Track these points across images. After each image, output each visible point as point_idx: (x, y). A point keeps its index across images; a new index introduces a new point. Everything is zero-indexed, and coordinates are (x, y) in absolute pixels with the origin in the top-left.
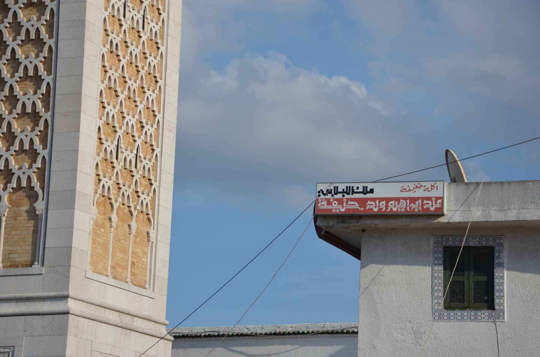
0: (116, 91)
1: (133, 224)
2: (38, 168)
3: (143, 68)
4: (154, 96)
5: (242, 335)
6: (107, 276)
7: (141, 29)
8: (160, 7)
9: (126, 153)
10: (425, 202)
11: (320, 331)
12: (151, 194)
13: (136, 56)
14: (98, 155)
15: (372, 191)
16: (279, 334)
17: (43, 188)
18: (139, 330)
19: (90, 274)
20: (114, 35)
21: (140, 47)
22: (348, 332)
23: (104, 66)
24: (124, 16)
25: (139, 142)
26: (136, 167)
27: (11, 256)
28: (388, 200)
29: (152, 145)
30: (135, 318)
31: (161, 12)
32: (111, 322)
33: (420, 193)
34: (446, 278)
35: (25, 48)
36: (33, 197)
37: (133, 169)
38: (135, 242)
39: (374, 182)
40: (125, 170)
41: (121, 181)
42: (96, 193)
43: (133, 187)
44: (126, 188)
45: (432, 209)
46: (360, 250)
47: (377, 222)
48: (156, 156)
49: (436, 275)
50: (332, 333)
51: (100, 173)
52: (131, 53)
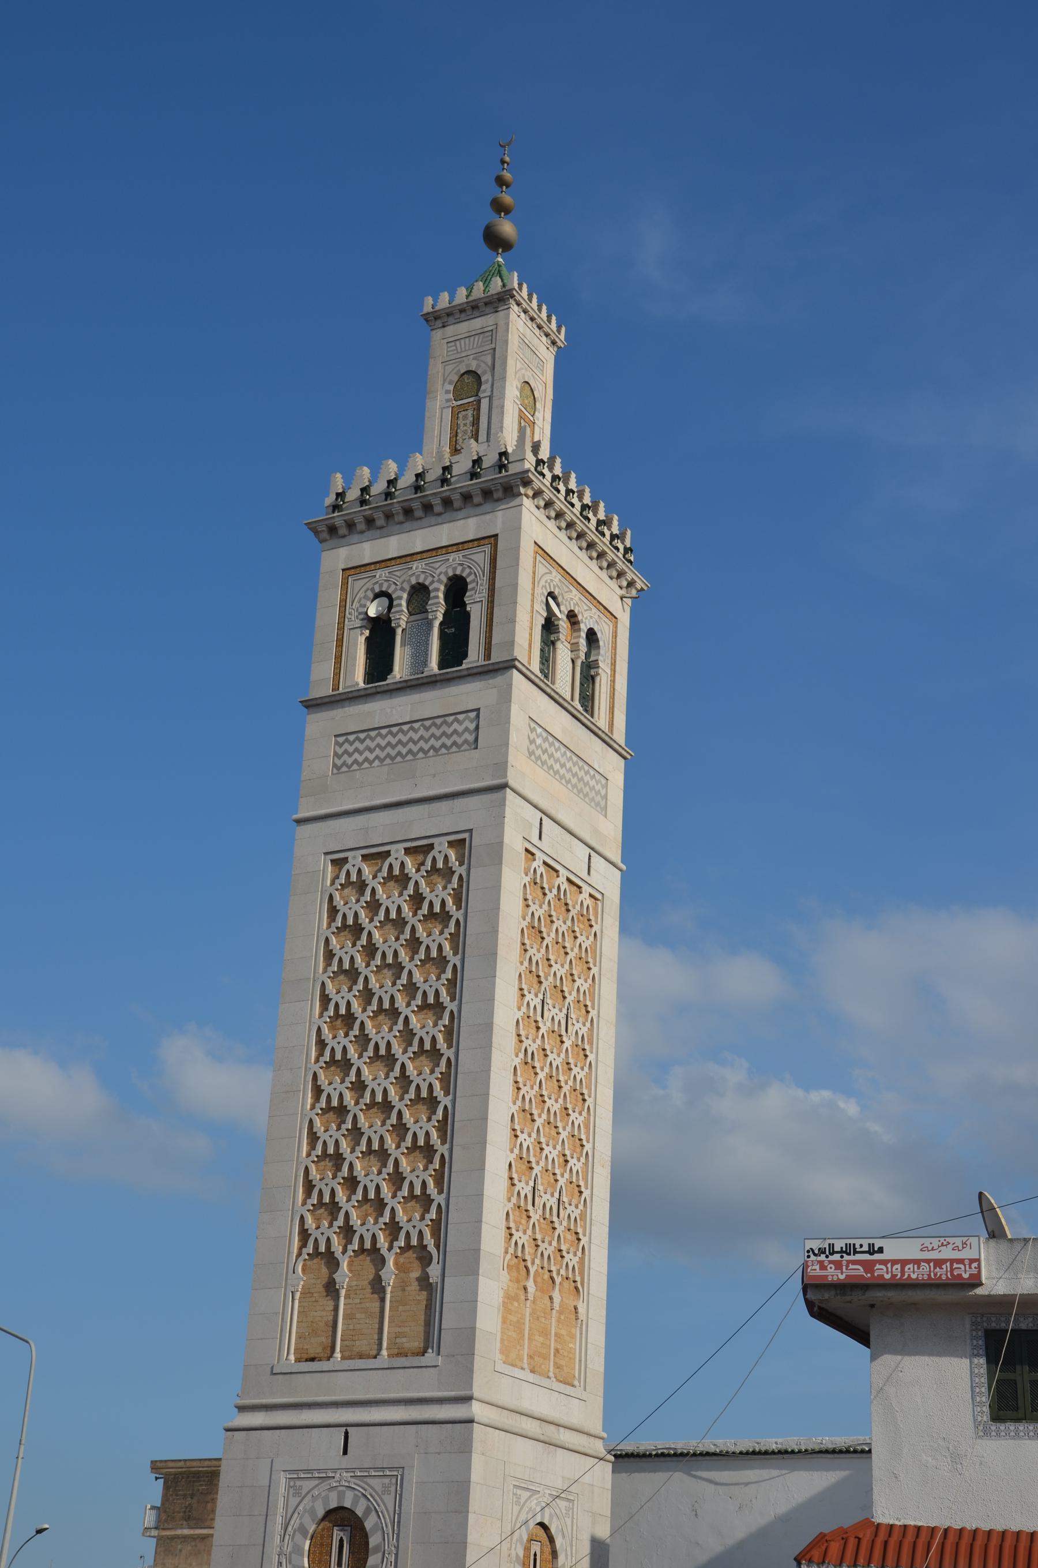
0: (531, 1114)
1: (556, 1295)
2: (431, 1220)
3: (566, 1083)
4: (581, 1119)
5: (708, 1454)
6: (522, 1368)
7: (563, 1033)
8: (588, 1003)
9: (545, 1197)
10: (955, 1265)
11: (817, 1448)
12: (579, 1254)
13: (557, 1067)
14: (509, 1200)
15: (881, 1250)
16: (760, 1453)
17: (437, 1246)
18: (567, 1446)
20: (530, 1041)
21: (563, 1055)
22: (855, 1452)
24: (542, 1017)
25: (562, 1182)
26: (558, 1217)
27: (398, 1340)
28: (904, 1263)
29: (579, 1186)
30: (561, 1429)
31: (589, 1009)
32: (530, 1434)
33: (947, 1253)
34: (991, 1375)
35: (418, 1062)
36: (425, 1259)
37: (555, 1219)
38: (558, 1321)
39: (883, 1237)
40: (545, 1222)
41: (538, 1236)
42: (506, 1252)
43: (555, 1243)
44: (546, 1245)
45: (966, 1276)
46: (869, 1335)
47: (891, 1294)
48: (585, 1200)
49: (976, 1371)
50: (834, 1452)
51: (512, 1225)
52: (551, 1063)
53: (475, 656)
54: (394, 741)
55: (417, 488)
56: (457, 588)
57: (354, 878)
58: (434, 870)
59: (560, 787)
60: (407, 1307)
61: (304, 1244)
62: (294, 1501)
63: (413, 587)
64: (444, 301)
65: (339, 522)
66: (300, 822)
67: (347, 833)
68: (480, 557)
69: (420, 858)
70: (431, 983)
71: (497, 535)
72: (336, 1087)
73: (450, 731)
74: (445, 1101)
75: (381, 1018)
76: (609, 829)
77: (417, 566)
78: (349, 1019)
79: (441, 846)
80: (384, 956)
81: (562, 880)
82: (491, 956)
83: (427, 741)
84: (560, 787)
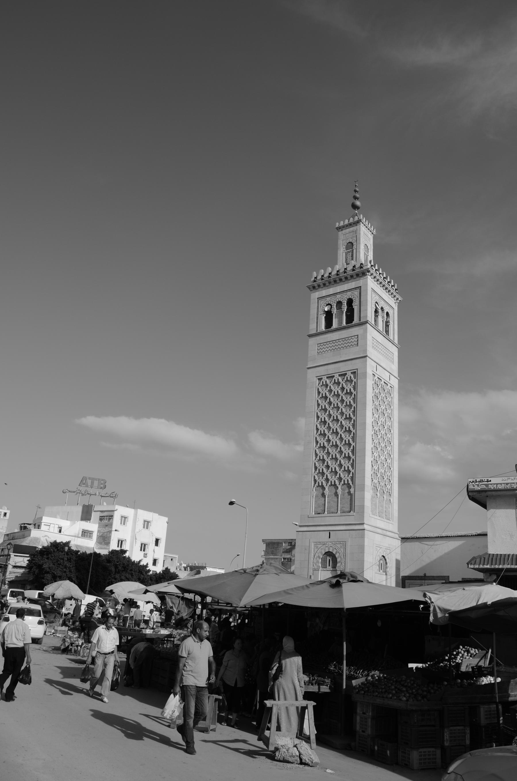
15: (490, 481)
19: (371, 515)
25: (385, 466)
28: (497, 484)
33: (509, 481)
36: (349, 487)
47: (493, 493)
50: (461, 536)
53: (356, 320)
55: (337, 275)
56: (350, 302)
57: (324, 383)
58: (347, 380)
59: (381, 356)
61: (315, 483)
62: (316, 550)
63: (337, 302)
64: (342, 223)
65: (316, 285)
66: (308, 368)
67: (322, 371)
68: (357, 293)
69: (343, 377)
70: (348, 412)
72: (322, 441)
73: (350, 341)
74: (353, 444)
75: (334, 422)
76: (394, 368)
77: (338, 296)
78: (325, 422)
79: (349, 374)
80: (334, 405)
81: (382, 382)
82: (365, 404)
84: (381, 356)
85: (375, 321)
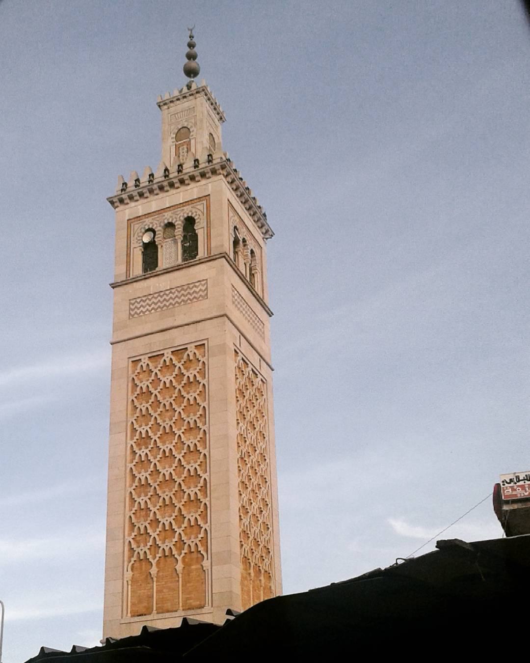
23: (239, 467)
27: (188, 601)
42: (241, 554)
53: (202, 253)
54: (161, 300)
60: (191, 584)
65: (124, 196)
71: (209, 195)
79: (191, 349)
83: (179, 298)
85: (235, 253)
